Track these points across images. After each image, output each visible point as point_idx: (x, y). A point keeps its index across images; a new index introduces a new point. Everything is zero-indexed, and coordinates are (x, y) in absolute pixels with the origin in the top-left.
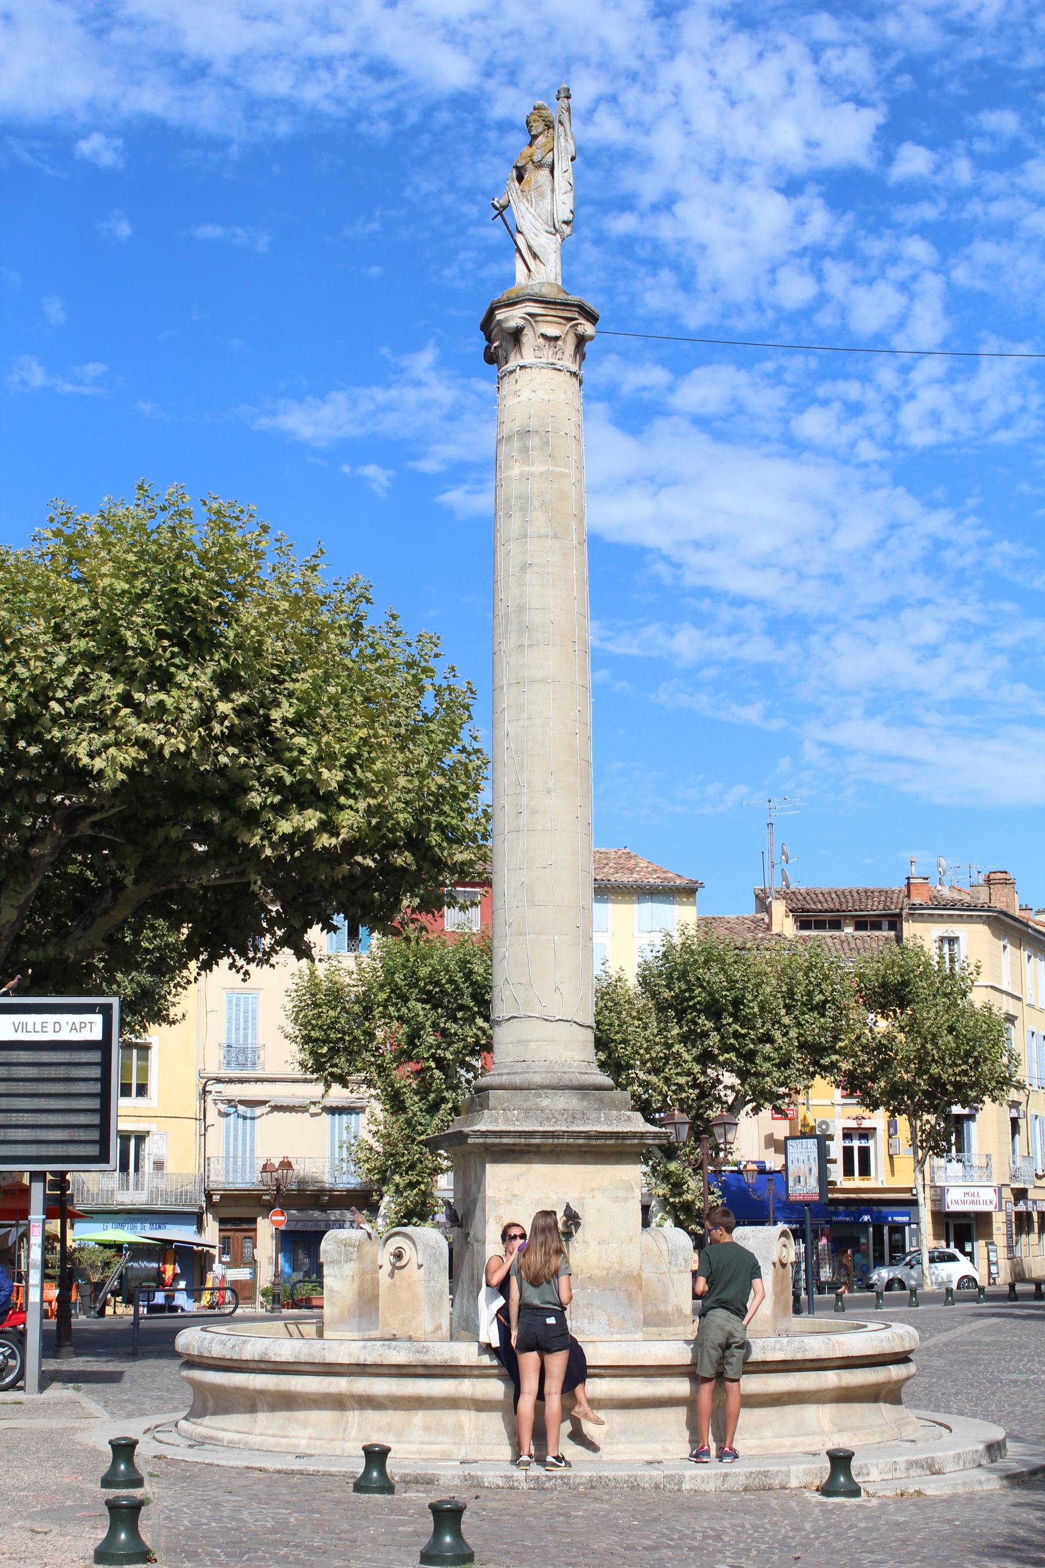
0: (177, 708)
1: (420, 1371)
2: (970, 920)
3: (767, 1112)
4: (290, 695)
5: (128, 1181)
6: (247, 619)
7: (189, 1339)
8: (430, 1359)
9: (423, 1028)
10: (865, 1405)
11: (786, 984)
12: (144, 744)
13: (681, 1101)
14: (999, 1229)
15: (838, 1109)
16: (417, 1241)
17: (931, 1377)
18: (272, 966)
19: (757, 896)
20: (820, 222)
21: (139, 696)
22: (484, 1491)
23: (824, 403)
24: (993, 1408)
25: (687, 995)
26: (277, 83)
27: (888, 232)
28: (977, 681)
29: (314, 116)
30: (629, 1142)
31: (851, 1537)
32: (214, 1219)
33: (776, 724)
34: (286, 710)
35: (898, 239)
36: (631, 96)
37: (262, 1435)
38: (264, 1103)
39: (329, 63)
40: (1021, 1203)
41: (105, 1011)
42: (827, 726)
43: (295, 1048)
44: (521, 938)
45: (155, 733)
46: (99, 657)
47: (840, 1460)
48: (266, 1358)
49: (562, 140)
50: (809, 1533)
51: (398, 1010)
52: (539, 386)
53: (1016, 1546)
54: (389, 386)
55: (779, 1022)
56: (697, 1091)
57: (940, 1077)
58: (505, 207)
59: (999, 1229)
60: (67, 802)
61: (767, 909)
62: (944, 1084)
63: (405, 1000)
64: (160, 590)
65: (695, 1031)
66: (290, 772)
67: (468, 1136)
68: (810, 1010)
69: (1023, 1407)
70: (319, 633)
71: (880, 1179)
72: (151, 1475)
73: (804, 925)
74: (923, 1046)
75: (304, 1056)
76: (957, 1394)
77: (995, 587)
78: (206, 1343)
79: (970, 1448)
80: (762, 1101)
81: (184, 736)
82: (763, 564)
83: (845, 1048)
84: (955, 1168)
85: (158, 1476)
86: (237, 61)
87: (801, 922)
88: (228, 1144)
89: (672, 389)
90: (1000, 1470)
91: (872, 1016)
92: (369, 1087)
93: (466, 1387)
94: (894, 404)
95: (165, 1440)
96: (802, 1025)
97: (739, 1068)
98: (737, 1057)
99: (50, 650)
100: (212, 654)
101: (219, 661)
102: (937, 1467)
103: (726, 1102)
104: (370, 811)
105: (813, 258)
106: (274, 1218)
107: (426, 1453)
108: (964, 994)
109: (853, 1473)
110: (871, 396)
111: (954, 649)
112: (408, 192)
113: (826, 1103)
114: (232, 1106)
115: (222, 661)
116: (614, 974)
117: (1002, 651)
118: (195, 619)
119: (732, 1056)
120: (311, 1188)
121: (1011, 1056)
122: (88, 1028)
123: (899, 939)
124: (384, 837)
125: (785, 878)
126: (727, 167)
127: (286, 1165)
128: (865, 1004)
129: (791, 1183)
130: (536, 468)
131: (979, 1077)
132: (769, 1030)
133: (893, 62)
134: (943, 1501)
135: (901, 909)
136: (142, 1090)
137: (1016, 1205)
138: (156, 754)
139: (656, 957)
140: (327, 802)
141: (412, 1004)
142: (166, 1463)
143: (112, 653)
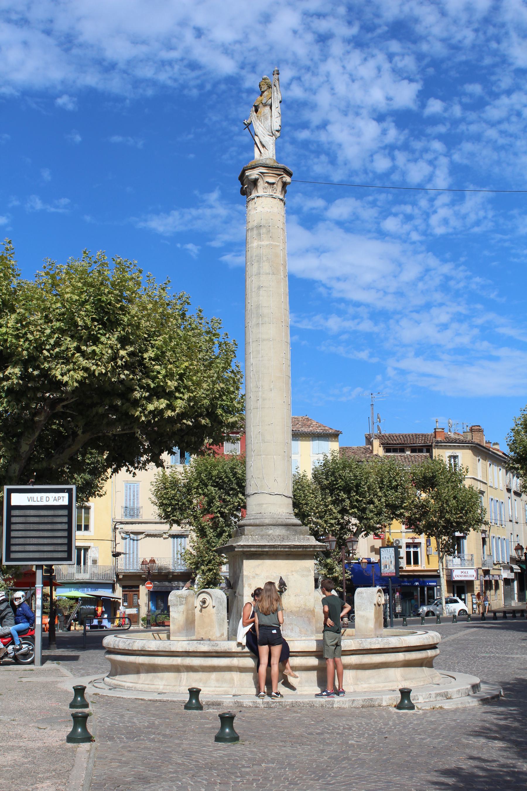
0: (101, 353)
1: (214, 654)
2: (463, 448)
3: (371, 536)
5: (80, 569)
6: (133, 312)
7: (109, 641)
9: (215, 498)
12: (86, 369)
13: (332, 531)
15: (404, 534)
16: (212, 596)
18: (146, 470)
19: (366, 437)
20: (393, 134)
21: (84, 348)
23: (396, 215)
25: (335, 483)
26: (147, 72)
27: (424, 138)
28: (465, 340)
29: (164, 87)
30: (308, 550)
32: (120, 586)
33: (375, 360)
34: (151, 353)
36: (307, 77)
37: (142, 684)
39: (171, 63)
40: (487, 576)
41: (70, 491)
42: (398, 361)
43: (157, 508)
44: (259, 457)
45: (91, 364)
46: (66, 330)
47: (405, 693)
48: (144, 649)
49: (275, 93)
52: (266, 206)
54: (198, 208)
55: (376, 495)
56: (339, 527)
57: (450, 519)
60: (51, 396)
61: (371, 444)
62: (452, 523)
63: (206, 486)
64: (93, 299)
65: (338, 499)
66: (153, 382)
67: (235, 547)
68: (391, 489)
69: (488, 668)
70: (165, 317)
71: (423, 566)
74: (442, 505)
76: (458, 663)
79: (464, 687)
82: (368, 287)
83: (407, 506)
84: (457, 560)
86: (128, 62)
87: (386, 449)
89: (326, 209)
91: (419, 492)
92: (190, 525)
93: (235, 662)
94: (427, 215)
96: (387, 496)
98: (358, 510)
99: (43, 327)
100: (117, 329)
101: (120, 332)
103: (353, 531)
104: (189, 400)
105: (390, 150)
106: (147, 585)
107: (217, 691)
108: (461, 481)
110: (416, 211)
111: (455, 326)
112: (206, 121)
113: (398, 531)
115: (122, 332)
117: (477, 326)
120: (164, 572)
121: (482, 510)
122: (63, 499)
123: (431, 456)
124: (196, 411)
125: (379, 429)
126: (350, 109)
127: (153, 561)
128: (415, 486)
129: (382, 568)
130: (265, 243)
134: (452, 711)
135: (432, 443)
136: (87, 528)
137: (484, 577)
138: (91, 374)
140: (170, 396)
143: (71, 328)
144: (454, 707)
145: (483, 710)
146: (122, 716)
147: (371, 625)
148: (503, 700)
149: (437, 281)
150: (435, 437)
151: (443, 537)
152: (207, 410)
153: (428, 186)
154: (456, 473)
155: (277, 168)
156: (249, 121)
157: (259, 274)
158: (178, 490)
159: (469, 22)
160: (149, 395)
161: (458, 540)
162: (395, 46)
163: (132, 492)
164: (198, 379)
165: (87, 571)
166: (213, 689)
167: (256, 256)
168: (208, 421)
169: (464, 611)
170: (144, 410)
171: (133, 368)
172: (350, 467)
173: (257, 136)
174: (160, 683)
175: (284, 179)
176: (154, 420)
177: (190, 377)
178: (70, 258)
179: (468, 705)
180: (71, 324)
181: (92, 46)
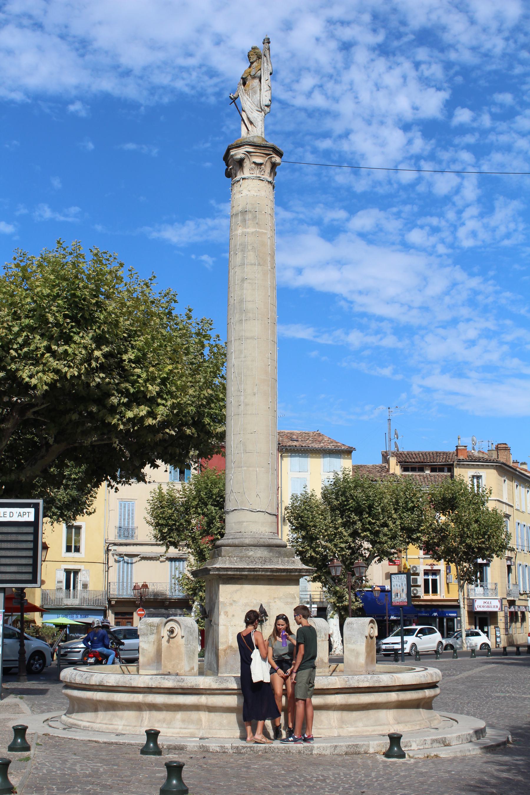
0: (74, 354)
1: (180, 691)
2: (487, 467)
3: (385, 562)
4: (133, 347)
5: (69, 594)
6: (110, 308)
8: (184, 685)
9: (215, 519)
10: (412, 710)
11: (395, 498)
12: (57, 371)
13: (342, 556)
14: (501, 620)
15: (422, 560)
16: (181, 624)
17: (457, 694)
18: (130, 484)
19: (383, 455)
20: (419, 144)
21: (54, 347)
22: (210, 754)
23: (422, 227)
24: (485, 711)
25: (346, 503)
27: (451, 148)
28: (494, 357)
29: (182, 95)
30: (293, 574)
31: (395, 780)
32: (112, 613)
33: (399, 377)
34: (131, 355)
35: (456, 152)
36: (330, 86)
37: (100, 723)
38: (137, 555)
40: (512, 607)
41: (36, 506)
42: (423, 378)
43: (151, 528)
44: (239, 469)
45: (63, 366)
46: (36, 328)
47: (395, 739)
48: (102, 684)
49: (265, 64)
50: (373, 778)
51: (202, 510)
52: (252, 189)
53: (481, 786)
54: (214, 218)
55: (391, 517)
56: (350, 551)
57: (471, 545)
58: (236, 98)
59: (501, 620)
60: (19, 401)
62: (473, 548)
63: (206, 505)
64: (66, 294)
65: (349, 521)
66: (132, 386)
67: (210, 570)
68: (407, 511)
69: (501, 710)
70: (150, 315)
71: (442, 595)
72: (37, 744)
73: (405, 469)
74: (463, 530)
75: (154, 532)
76: (468, 703)
77: (502, 313)
78: (73, 676)
79: (466, 733)
80: (383, 556)
81: (77, 367)
83: (424, 530)
84: (479, 590)
85: (41, 745)
86: (145, 69)
87: (404, 468)
88: (119, 576)
89: (348, 220)
90: (481, 744)
91: (438, 514)
92: (188, 548)
94: (454, 228)
95: (53, 725)
96: (402, 518)
97: (371, 539)
98: (370, 534)
99: (10, 324)
100: (92, 326)
101: (95, 330)
102: (447, 742)
103: (365, 556)
104: (173, 406)
106: (139, 612)
107: (182, 734)
108: (483, 504)
109: (402, 745)
111: (483, 342)
112: (224, 129)
113: (415, 557)
114: (121, 557)
115: (97, 330)
116: (310, 492)
117: (507, 343)
118: (84, 309)
119: (368, 533)
120: (160, 598)
121: (507, 535)
122: (29, 515)
123: (452, 476)
124: (181, 420)
125: (396, 446)
127: (145, 586)
128: (434, 508)
129: (393, 597)
130: (250, 230)
131: (490, 545)
132: (386, 521)
133: (457, 68)
134: (448, 760)
135: (454, 462)
136: (77, 550)
137: (509, 608)
138: (63, 377)
139: (331, 485)
141: (209, 507)
142: (49, 738)
143: (41, 325)
144: (452, 755)
145: (485, 759)
146: (65, 761)
147: (362, 660)
148: (510, 748)
149: (464, 295)
150: (457, 455)
151: (464, 564)
152: (193, 418)
153: (456, 199)
154: (478, 494)
155: (265, 147)
156: (235, 96)
157: (243, 264)
158: (176, 509)
159: (500, 31)
160: (128, 401)
161: (481, 568)
162: (422, 54)
163: (126, 508)
164: (183, 383)
165: (77, 595)
166: (178, 730)
167: (240, 245)
168: (194, 430)
169: (486, 645)
170: (121, 417)
171: (109, 371)
172: (362, 486)
173: (244, 111)
174: (119, 723)
175: (273, 160)
176: (133, 428)
177: (174, 381)
178: (44, 249)
179: (469, 754)
180: (42, 322)
181: (107, 52)
